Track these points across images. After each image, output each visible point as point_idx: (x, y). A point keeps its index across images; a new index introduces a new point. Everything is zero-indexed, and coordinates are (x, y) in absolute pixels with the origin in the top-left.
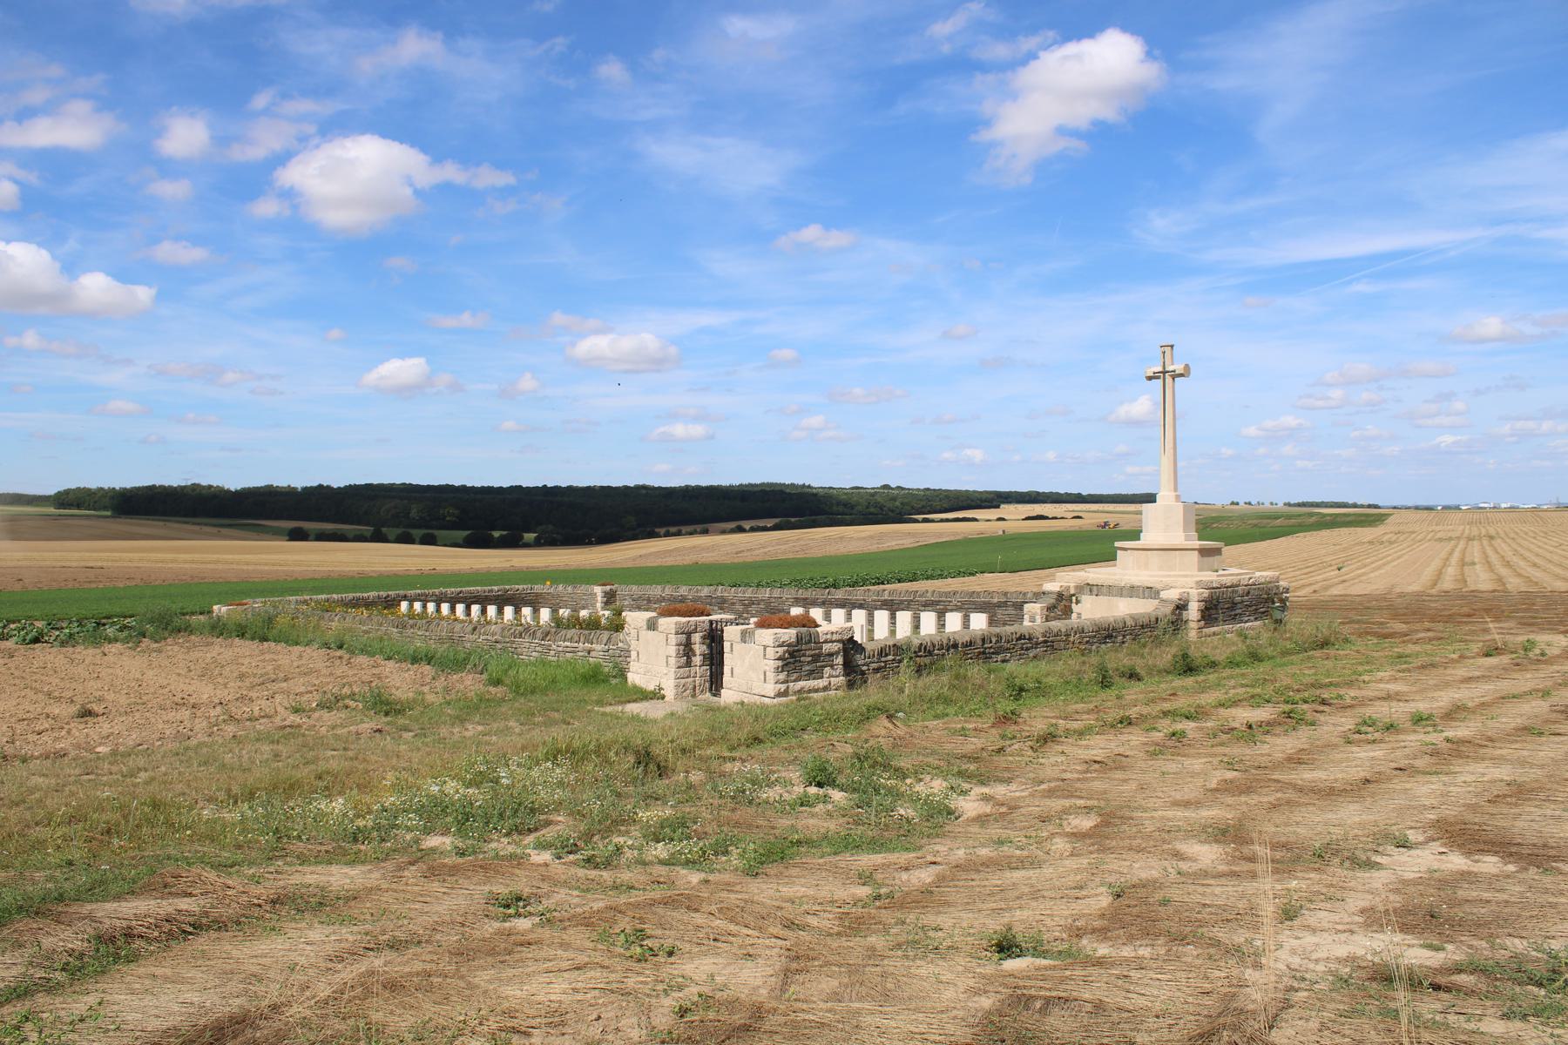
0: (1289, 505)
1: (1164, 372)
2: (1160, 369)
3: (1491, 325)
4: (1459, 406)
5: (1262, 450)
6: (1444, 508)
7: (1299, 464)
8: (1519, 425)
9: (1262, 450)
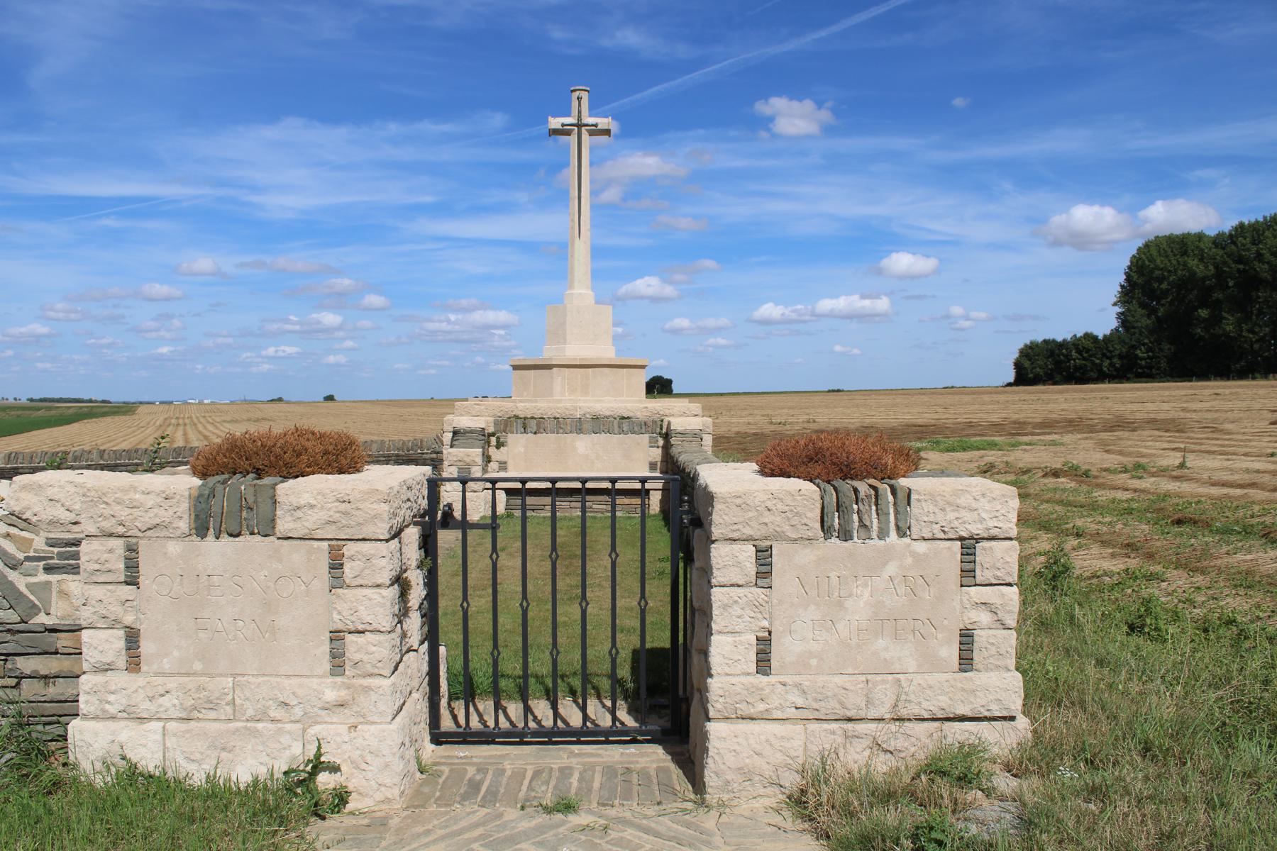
0: (31, 400)
1: (579, 125)
2: (574, 121)
3: (204, 263)
4: (176, 323)
5: (10, 353)
6: (161, 403)
7: (39, 365)
8: (220, 340)
9: (10, 353)
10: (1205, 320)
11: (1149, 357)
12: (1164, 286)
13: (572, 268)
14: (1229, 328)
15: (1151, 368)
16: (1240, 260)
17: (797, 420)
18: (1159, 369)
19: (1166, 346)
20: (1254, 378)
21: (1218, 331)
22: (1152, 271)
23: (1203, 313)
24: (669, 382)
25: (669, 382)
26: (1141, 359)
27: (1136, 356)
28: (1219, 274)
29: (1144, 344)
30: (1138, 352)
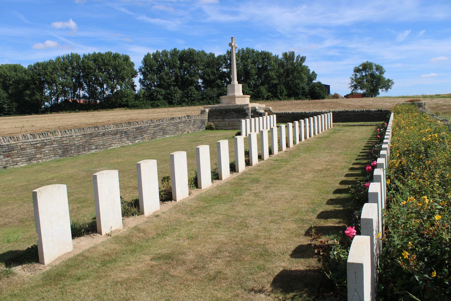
10: (29, 95)
11: (8, 108)
12: (11, 82)
13: (60, 258)
14: (38, 97)
15: (9, 111)
16: (39, 75)
17: (198, 177)
18: (13, 112)
19: (14, 104)
20: (47, 114)
21: (34, 98)
22: (6, 77)
23: (28, 92)
24: (328, 87)
25: (328, 87)
26: (6, 108)
27: (4, 107)
28: (33, 79)
29: (6, 103)
30: (4, 106)
